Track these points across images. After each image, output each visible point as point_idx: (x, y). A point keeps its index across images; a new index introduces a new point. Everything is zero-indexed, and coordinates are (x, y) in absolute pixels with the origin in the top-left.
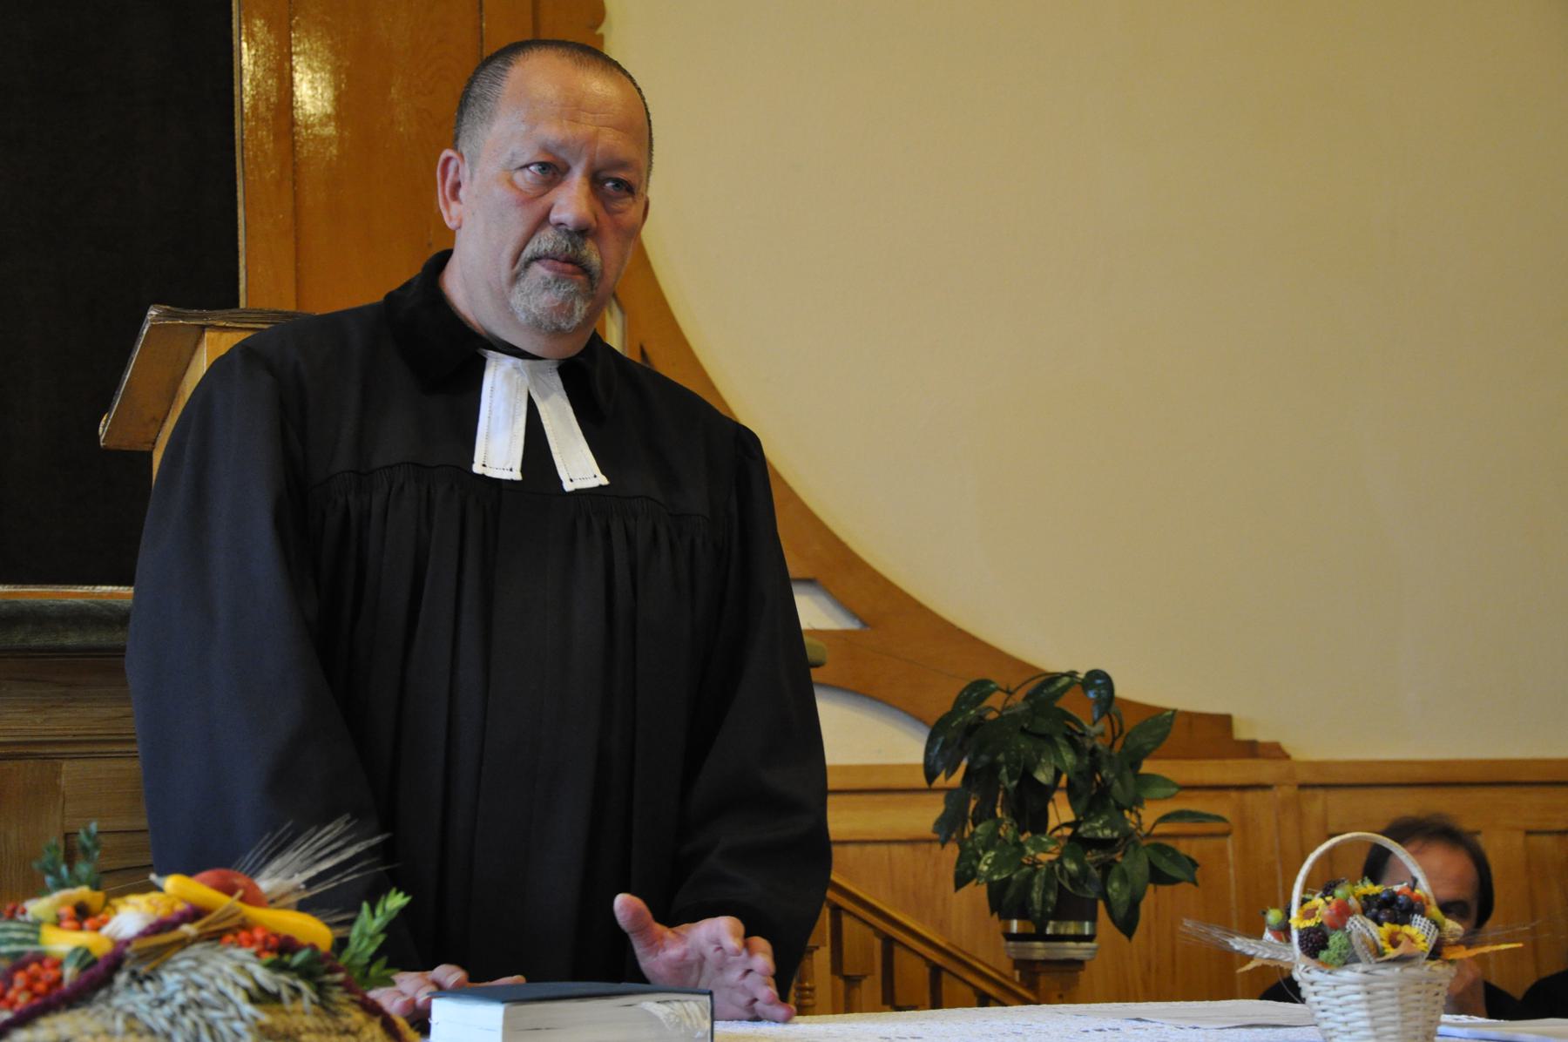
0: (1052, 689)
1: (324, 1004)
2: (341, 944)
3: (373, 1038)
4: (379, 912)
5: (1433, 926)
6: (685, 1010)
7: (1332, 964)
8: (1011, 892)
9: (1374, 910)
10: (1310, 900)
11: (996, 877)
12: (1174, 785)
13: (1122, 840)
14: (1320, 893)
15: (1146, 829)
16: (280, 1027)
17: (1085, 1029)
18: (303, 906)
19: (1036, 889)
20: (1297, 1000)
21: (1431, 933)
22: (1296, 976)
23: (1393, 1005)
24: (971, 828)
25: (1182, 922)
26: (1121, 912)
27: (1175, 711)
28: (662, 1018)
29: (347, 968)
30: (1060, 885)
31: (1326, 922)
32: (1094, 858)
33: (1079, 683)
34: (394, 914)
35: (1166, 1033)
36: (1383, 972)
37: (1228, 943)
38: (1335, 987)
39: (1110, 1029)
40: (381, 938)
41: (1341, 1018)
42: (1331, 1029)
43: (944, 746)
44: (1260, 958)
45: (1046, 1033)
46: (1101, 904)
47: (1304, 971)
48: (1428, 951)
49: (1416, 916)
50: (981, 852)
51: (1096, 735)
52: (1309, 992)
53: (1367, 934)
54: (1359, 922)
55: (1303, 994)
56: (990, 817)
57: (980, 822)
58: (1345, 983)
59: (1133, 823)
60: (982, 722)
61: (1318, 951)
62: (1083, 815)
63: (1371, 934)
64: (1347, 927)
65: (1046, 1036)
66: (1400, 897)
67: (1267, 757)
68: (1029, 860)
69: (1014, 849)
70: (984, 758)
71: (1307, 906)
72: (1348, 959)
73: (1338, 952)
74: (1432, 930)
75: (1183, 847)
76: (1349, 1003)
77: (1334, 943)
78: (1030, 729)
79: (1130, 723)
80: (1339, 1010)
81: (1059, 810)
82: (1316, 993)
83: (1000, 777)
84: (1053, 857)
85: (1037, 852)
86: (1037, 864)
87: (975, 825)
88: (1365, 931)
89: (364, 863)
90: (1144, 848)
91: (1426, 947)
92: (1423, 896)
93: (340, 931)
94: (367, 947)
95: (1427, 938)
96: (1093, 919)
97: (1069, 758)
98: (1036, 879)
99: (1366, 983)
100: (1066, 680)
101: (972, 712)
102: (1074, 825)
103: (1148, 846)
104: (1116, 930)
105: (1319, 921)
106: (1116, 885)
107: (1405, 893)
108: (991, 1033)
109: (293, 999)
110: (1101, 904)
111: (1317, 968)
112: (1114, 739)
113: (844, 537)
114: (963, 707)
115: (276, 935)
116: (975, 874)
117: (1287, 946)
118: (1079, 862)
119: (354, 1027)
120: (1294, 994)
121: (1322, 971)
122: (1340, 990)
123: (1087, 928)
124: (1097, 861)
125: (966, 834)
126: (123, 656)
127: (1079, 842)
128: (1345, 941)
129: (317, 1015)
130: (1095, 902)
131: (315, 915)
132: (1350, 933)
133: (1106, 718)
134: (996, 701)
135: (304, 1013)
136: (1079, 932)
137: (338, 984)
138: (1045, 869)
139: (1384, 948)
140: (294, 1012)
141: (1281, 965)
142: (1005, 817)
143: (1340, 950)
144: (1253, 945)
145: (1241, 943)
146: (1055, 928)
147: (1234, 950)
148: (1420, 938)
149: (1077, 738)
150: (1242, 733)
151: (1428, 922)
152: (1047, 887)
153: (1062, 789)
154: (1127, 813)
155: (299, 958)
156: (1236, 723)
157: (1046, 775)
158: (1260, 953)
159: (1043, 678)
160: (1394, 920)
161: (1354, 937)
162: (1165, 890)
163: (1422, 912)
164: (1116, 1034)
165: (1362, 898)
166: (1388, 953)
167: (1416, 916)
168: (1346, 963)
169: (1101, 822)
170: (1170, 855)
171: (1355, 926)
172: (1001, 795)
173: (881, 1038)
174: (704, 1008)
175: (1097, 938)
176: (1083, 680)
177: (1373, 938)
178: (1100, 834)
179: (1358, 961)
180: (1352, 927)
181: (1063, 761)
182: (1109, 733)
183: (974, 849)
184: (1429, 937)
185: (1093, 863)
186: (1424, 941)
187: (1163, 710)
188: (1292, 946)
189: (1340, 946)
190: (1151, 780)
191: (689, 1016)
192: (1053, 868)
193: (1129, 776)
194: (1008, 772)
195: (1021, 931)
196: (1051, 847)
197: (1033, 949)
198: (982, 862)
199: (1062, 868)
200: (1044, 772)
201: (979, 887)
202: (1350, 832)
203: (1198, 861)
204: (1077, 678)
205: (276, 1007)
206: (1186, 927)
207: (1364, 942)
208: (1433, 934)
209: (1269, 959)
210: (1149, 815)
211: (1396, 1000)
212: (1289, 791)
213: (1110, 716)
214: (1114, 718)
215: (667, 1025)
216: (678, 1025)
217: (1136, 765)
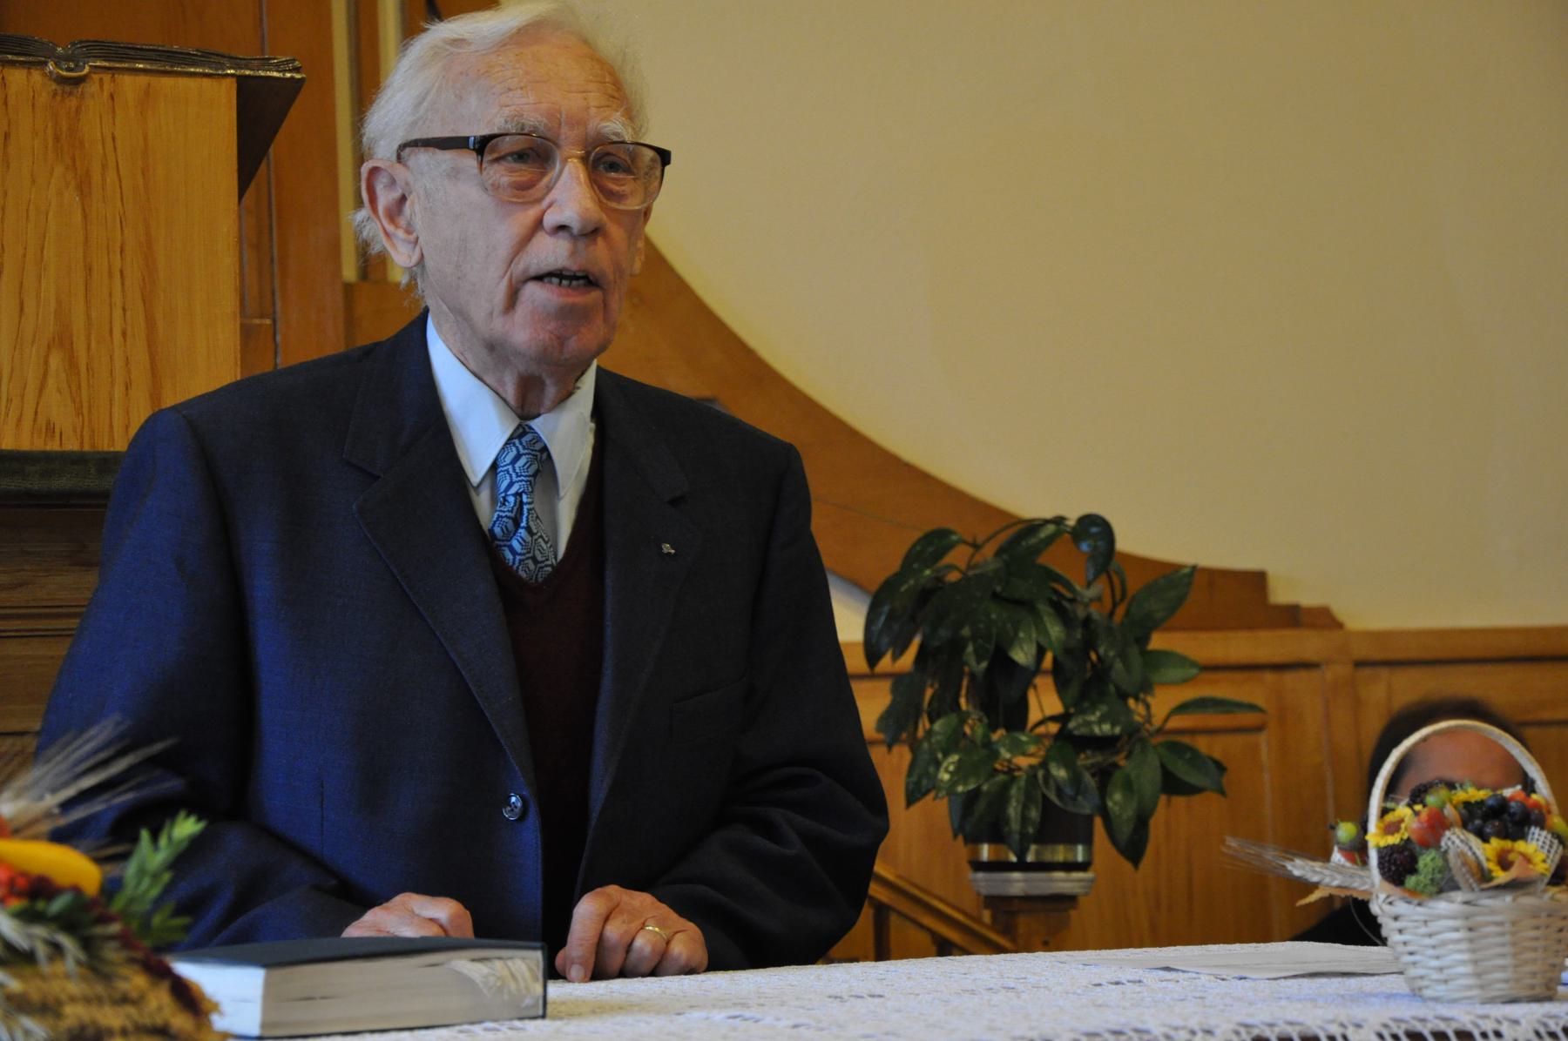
0: (1033, 541)
1: (95, 967)
2: (111, 888)
4: (163, 841)
5: (1556, 842)
6: (509, 969)
7: (1422, 892)
8: (981, 806)
9: (1478, 822)
10: (1393, 810)
11: (960, 789)
12: (1194, 664)
13: (1125, 738)
14: (1407, 800)
15: (1157, 721)
16: (35, 996)
17: (1096, 982)
18: (60, 836)
19: (1014, 803)
20: (1378, 942)
21: (1553, 851)
22: (1375, 908)
23: (1503, 945)
24: (927, 725)
25: (1224, 840)
26: (1125, 831)
27: (1194, 568)
28: (478, 981)
29: (123, 916)
30: (1044, 796)
31: (1414, 838)
32: (1090, 762)
33: (1069, 533)
34: (185, 844)
35: (1203, 986)
36: (1488, 902)
37: (1284, 866)
38: (1426, 922)
39: (1129, 981)
41: (1435, 963)
42: (1422, 978)
43: (891, 617)
44: (1328, 885)
45: (1045, 987)
46: (1098, 822)
47: (1384, 902)
48: (1549, 875)
49: (1533, 829)
50: (940, 756)
51: (1091, 600)
52: (1393, 930)
53: (1470, 854)
54: (1458, 837)
55: (1384, 933)
56: (953, 710)
57: (939, 716)
58: (1440, 917)
59: (1139, 715)
60: (940, 585)
61: (1405, 877)
62: (1076, 705)
63: (1474, 853)
64: (1443, 844)
65: (1047, 992)
66: (1513, 804)
67: (1312, 626)
68: (1002, 765)
69: (984, 752)
70: (944, 633)
71: (1390, 817)
72: (1444, 885)
73: (1430, 876)
74: (1555, 847)
75: (1202, 744)
76: (1444, 944)
77: (1426, 865)
78: (1004, 595)
79: (1134, 584)
80: (1431, 952)
81: (1043, 701)
82: (1400, 931)
83: (965, 658)
84: (1034, 761)
85: (1014, 755)
86: (1014, 770)
87: (932, 721)
88: (1466, 849)
89: (140, 779)
90: (1155, 747)
91: (1546, 870)
92: (1542, 802)
93: (113, 870)
94: (147, 890)
95: (1548, 857)
96: (1088, 841)
97: (1055, 631)
98: (1014, 791)
99: (1467, 917)
100: (1051, 528)
101: (928, 572)
102: (1062, 719)
103: (1161, 745)
104: (1113, 851)
105: (1405, 837)
106: (1118, 796)
107: (1518, 799)
108: (974, 988)
109: (51, 959)
110: (1098, 822)
111: (1403, 899)
112: (1115, 605)
113: (753, 342)
114: (916, 566)
115: (24, 874)
116: (934, 786)
117: (1362, 870)
118: (1069, 765)
119: (134, 995)
120: (1374, 935)
121: (1409, 903)
122: (1433, 927)
123: (1080, 854)
124: (1093, 765)
125: (921, 733)
126: (105, 506)
127: (1068, 742)
128: (1440, 862)
129: (84, 979)
130: (1089, 820)
131: (76, 847)
132: (1446, 852)
133: (1104, 578)
134: (958, 557)
135: (67, 976)
136: (1070, 858)
137: (112, 938)
138: (1024, 777)
139: (1490, 871)
140: (55, 976)
141: (1355, 895)
142: (971, 709)
143: (1433, 874)
144: (1318, 869)
145: (1303, 868)
146: (1038, 853)
147: (1293, 876)
148: (1539, 857)
149: (1066, 604)
150: (1280, 595)
151: (1549, 836)
152: (1028, 800)
153: (1046, 672)
154: (1131, 702)
155: (57, 905)
156: (1273, 582)
157: (1026, 654)
158: (1327, 880)
159: (1020, 527)
160: (1504, 835)
161: (1451, 856)
162: (1180, 801)
163: (1541, 823)
164: (1137, 988)
165: (1461, 806)
166: (1498, 877)
167: (1533, 829)
168: (1441, 891)
169: (1098, 714)
170: (1188, 756)
171: (1453, 843)
172: (965, 683)
173: (830, 997)
174: (535, 968)
175: (1093, 867)
176: (1074, 528)
177: (1477, 858)
178: (1097, 730)
179: (1456, 888)
180: (1450, 843)
181: (1047, 633)
182: (1108, 601)
183: (932, 753)
184: (1551, 856)
185: (1087, 768)
186: (1544, 861)
187: (1175, 568)
188: (1369, 870)
189: (1433, 870)
190: (1158, 660)
191: (513, 976)
192: (1035, 776)
193: (1134, 652)
194: (976, 651)
195: (993, 858)
196: (1032, 749)
197: (1009, 881)
198: (942, 769)
199: (1048, 775)
200: (1022, 649)
201: (937, 801)
203: (1225, 764)
204: (1066, 526)
205: (28, 970)
206: (1229, 847)
207: (1465, 864)
208: (1556, 852)
209: (1339, 887)
210: (1161, 704)
211: (1507, 938)
212: (1339, 671)
213: (1109, 577)
214: (1116, 580)
215: (485, 991)
216: (500, 990)
217: (1143, 640)
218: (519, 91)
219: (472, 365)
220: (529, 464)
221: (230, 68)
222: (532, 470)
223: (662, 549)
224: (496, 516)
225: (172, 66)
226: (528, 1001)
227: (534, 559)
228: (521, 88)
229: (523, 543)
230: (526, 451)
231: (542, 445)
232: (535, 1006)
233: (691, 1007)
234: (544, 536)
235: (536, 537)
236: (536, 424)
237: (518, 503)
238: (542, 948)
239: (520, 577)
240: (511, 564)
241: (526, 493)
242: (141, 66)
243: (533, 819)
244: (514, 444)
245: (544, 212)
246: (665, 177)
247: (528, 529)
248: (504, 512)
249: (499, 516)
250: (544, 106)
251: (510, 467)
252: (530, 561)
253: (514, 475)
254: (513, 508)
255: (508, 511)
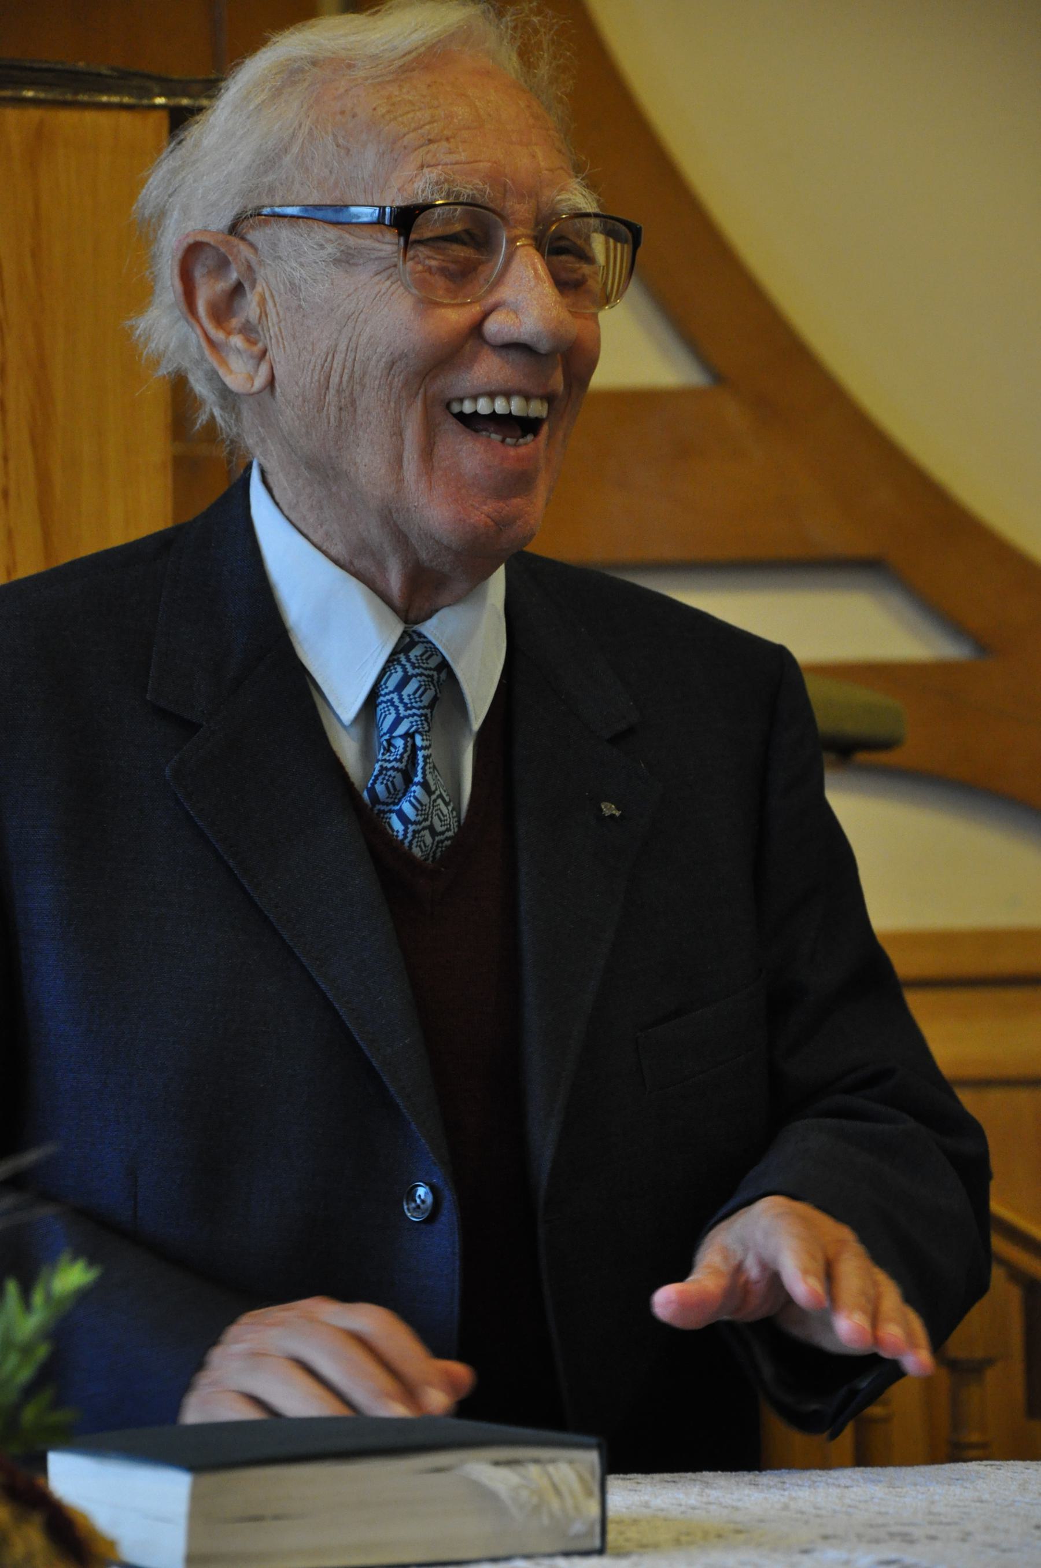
3: (29, 1557)
4: (38, 1298)
6: (550, 1477)
40: (42, 1351)
174: (587, 1476)
202: (412, 1221)
216: (537, 1509)
218: (444, 143)
219: (338, 549)
220: (422, 690)
221: (160, 95)
222: (426, 699)
223: (601, 810)
224: (377, 766)
225: (76, 93)
226: (578, 1527)
227: (431, 829)
228: (447, 139)
229: (417, 807)
230: (417, 671)
231: (438, 660)
232: (589, 1533)
233: (826, 1538)
234: (444, 794)
235: (434, 797)
236: (430, 629)
237: (409, 749)
238: (599, 1447)
239: (414, 857)
240: (401, 837)
241: (421, 734)
242: (30, 94)
243: (449, 1217)
244: (399, 663)
245: (486, 315)
246: (635, 268)
247: (425, 785)
248: (389, 761)
249: (382, 768)
250: (484, 166)
251: (395, 696)
252: (426, 833)
253: (401, 708)
254: (402, 755)
255: (395, 760)
